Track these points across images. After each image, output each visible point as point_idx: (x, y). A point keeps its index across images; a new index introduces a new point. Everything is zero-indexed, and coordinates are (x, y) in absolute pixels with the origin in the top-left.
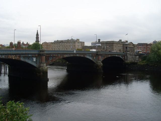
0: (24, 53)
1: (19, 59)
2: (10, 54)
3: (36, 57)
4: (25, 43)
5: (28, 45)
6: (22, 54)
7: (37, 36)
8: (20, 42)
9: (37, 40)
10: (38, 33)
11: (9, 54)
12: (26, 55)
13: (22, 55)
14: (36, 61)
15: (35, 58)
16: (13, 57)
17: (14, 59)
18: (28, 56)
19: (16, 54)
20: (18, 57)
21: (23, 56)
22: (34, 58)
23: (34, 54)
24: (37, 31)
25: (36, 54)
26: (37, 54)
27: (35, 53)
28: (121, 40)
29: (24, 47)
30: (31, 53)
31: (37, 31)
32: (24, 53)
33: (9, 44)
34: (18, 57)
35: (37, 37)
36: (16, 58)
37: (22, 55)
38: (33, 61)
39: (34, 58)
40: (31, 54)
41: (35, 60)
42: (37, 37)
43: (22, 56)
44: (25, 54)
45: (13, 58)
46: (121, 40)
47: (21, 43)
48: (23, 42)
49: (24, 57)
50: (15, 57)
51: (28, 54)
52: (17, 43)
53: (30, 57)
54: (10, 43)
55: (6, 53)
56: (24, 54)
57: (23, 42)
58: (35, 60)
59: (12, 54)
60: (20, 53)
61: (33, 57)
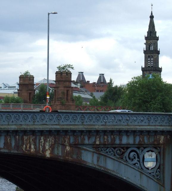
0: (98, 126)
1: (75, 156)
2: (33, 132)
3: (155, 147)
4: (92, 79)
5: (106, 89)
6: (89, 133)
7: (148, 45)
8: (69, 74)
9: (151, 64)
10: (157, 29)
11: (25, 132)
12: (108, 139)
13: (128, 136)
14: (160, 167)
15: (154, 155)
16: (44, 147)
17: (48, 154)
18: (117, 142)
19: (58, 132)
20: (70, 146)
21: (92, 140)
22: (147, 156)
23: (149, 132)
24: (152, 17)
25: (156, 132)
26: (162, 132)
27: (152, 128)
28: (89, 81)
29: (86, 100)
30: (132, 128)
31: (152, 17)
32: (97, 127)
33: (15, 82)
34: (68, 148)
35: (152, 48)
36: (59, 152)
37: (86, 138)
38: (142, 170)
39: (147, 156)
40: (134, 132)
41: (150, 165)
42: (152, 48)
43: (86, 142)
44: (105, 132)
45: (44, 150)
46: (89, 81)
47: (74, 78)
48: (81, 75)
49: (97, 148)
50: (52, 147)
51: (120, 132)
52: (53, 78)
53: (127, 147)
54: (21, 77)
55: (13, 127)
56: (97, 132)
57: (81, 75)
58: (150, 165)
59: (42, 132)
60: (81, 128)
61: (141, 146)
